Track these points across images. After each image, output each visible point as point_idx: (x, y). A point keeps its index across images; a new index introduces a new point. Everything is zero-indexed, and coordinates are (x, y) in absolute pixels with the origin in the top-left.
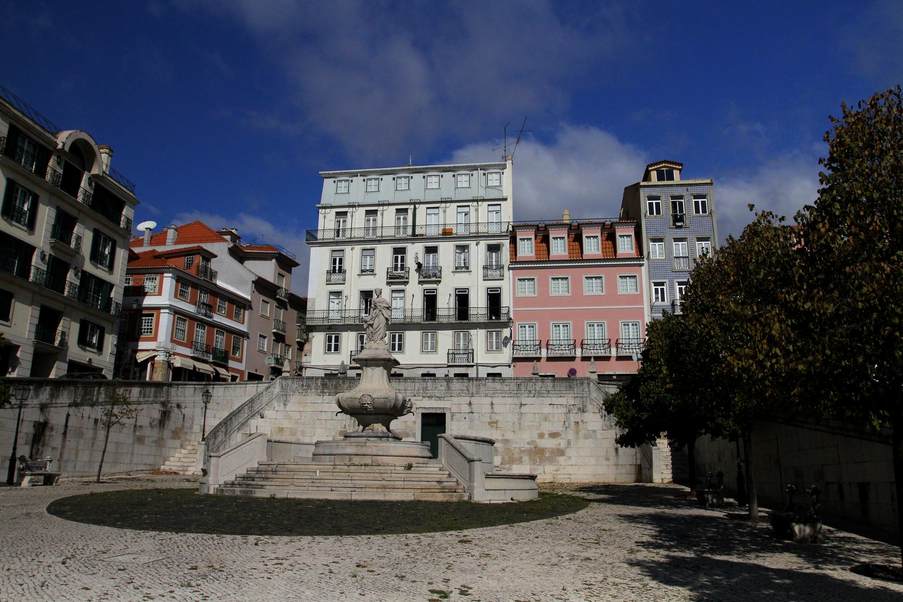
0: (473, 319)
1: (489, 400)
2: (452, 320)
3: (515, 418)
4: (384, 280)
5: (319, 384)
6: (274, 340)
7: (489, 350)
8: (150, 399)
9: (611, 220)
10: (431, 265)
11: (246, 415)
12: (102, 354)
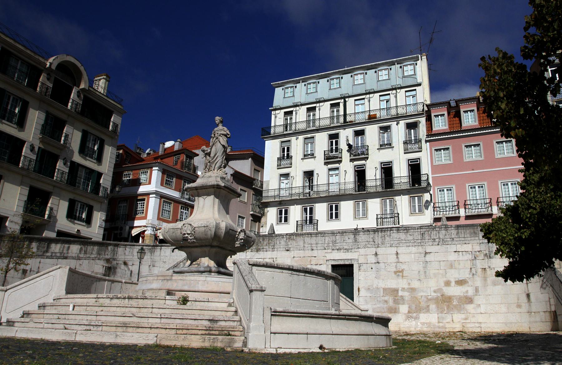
0: (396, 187)
1: (393, 250)
2: (379, 189)
3: (421, 267)
4: (323, 161)
6: (252, 220)
7: (412, 213)
8: (93, 256)
10: (360, 145)
12: (91, 227)
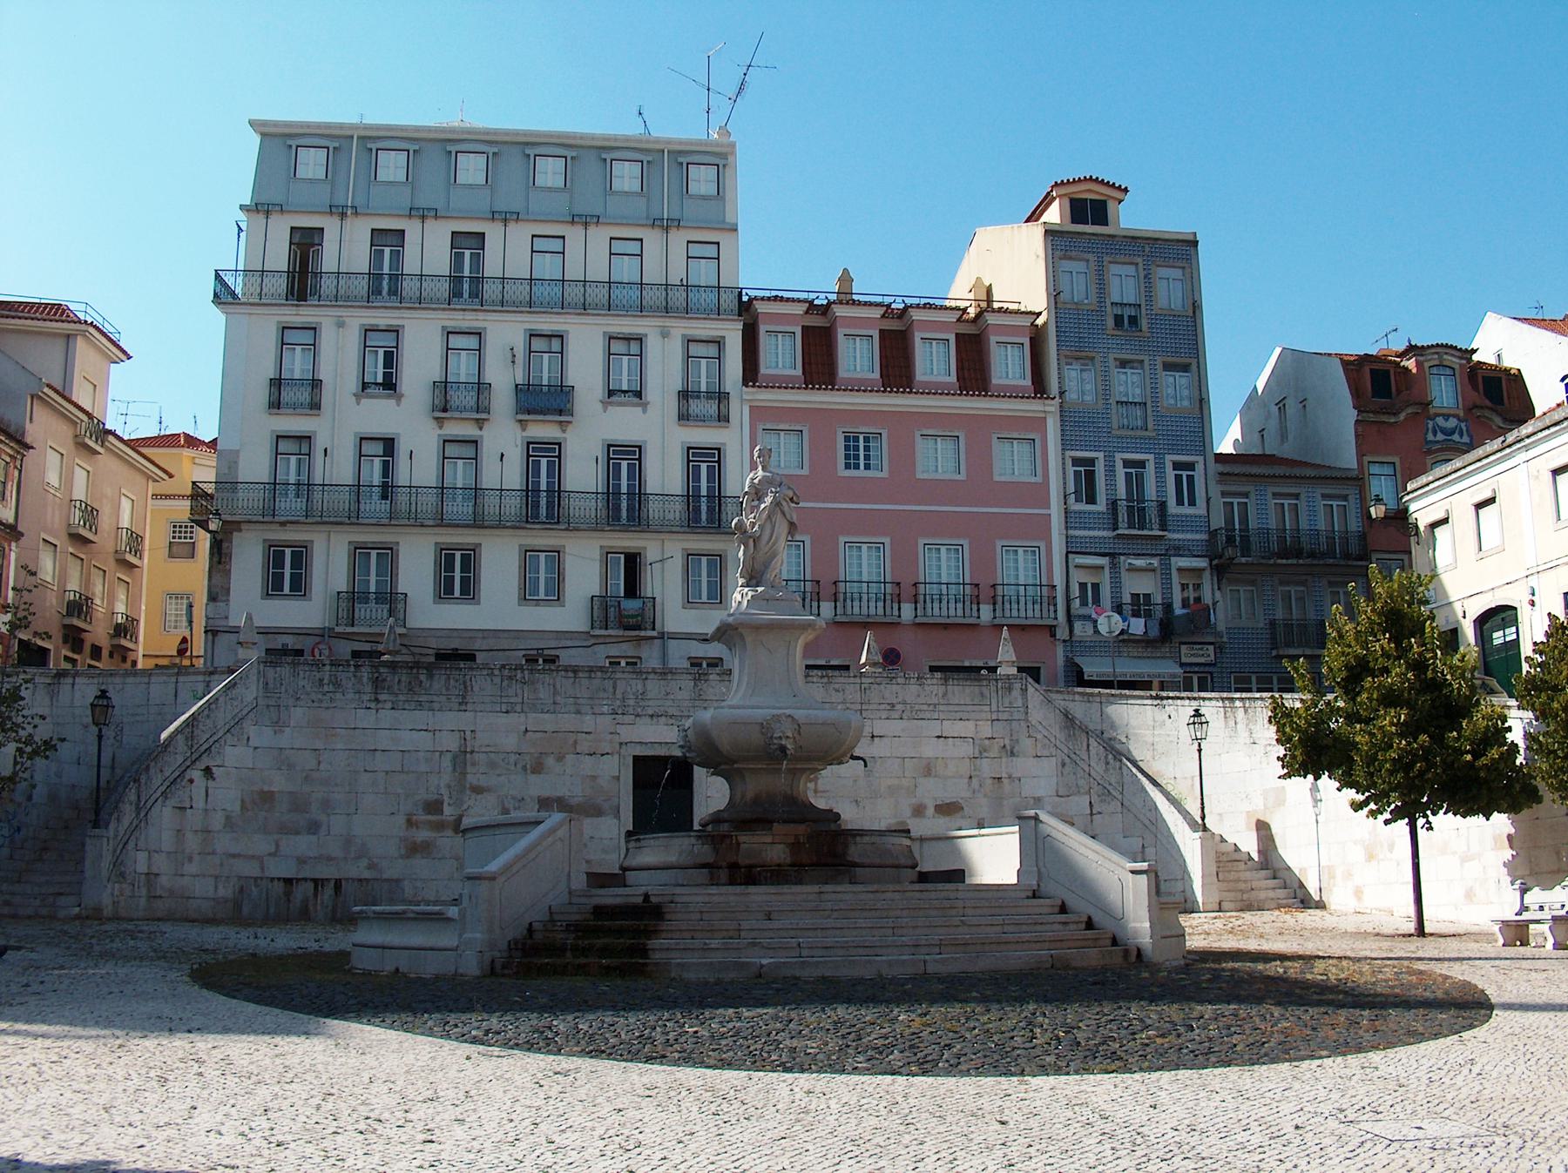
5: (365, 680)
9: (829, 295)
11: (180, 759)
